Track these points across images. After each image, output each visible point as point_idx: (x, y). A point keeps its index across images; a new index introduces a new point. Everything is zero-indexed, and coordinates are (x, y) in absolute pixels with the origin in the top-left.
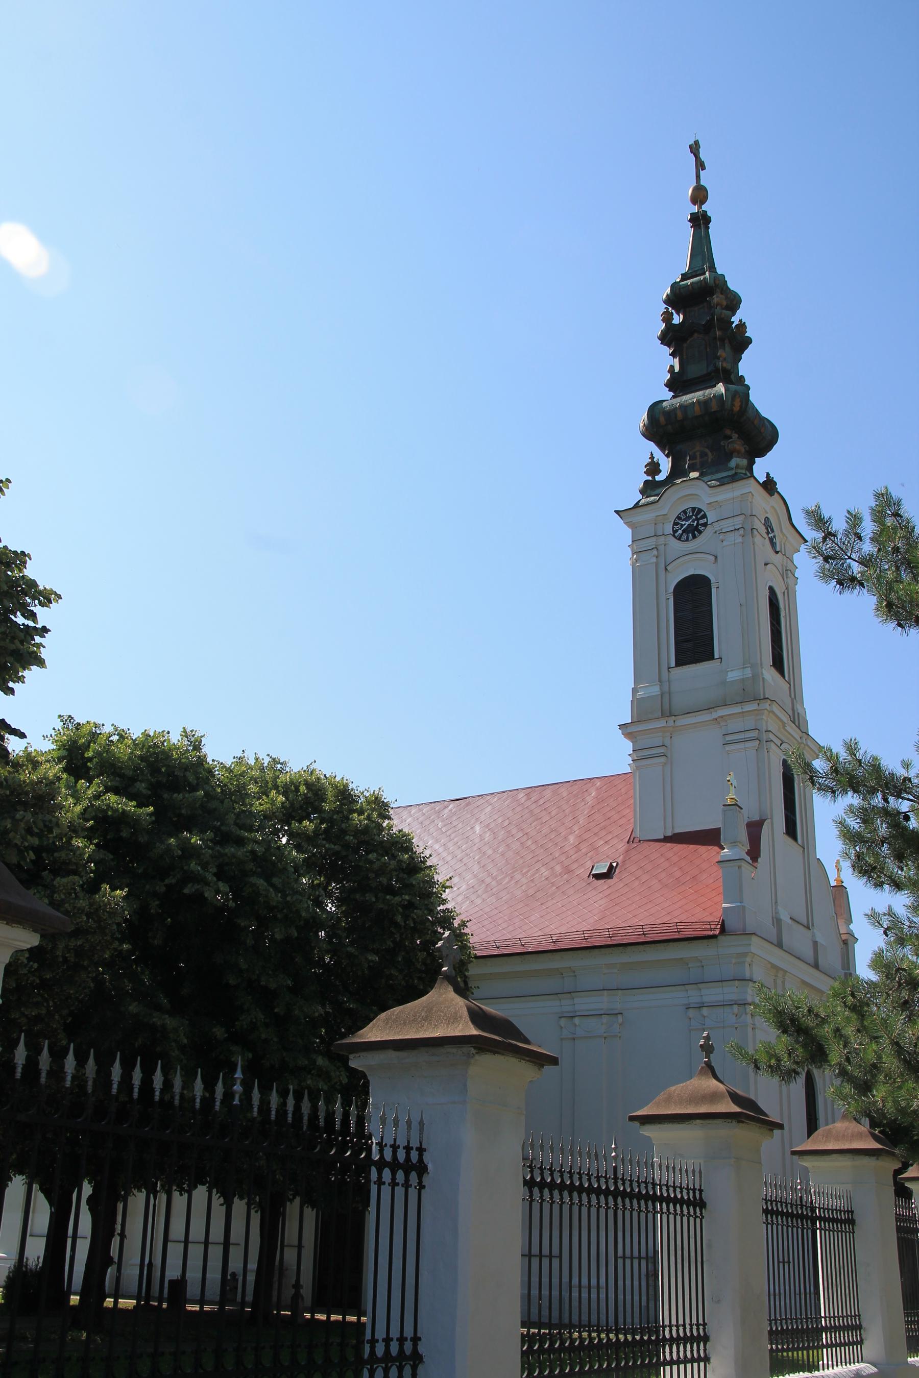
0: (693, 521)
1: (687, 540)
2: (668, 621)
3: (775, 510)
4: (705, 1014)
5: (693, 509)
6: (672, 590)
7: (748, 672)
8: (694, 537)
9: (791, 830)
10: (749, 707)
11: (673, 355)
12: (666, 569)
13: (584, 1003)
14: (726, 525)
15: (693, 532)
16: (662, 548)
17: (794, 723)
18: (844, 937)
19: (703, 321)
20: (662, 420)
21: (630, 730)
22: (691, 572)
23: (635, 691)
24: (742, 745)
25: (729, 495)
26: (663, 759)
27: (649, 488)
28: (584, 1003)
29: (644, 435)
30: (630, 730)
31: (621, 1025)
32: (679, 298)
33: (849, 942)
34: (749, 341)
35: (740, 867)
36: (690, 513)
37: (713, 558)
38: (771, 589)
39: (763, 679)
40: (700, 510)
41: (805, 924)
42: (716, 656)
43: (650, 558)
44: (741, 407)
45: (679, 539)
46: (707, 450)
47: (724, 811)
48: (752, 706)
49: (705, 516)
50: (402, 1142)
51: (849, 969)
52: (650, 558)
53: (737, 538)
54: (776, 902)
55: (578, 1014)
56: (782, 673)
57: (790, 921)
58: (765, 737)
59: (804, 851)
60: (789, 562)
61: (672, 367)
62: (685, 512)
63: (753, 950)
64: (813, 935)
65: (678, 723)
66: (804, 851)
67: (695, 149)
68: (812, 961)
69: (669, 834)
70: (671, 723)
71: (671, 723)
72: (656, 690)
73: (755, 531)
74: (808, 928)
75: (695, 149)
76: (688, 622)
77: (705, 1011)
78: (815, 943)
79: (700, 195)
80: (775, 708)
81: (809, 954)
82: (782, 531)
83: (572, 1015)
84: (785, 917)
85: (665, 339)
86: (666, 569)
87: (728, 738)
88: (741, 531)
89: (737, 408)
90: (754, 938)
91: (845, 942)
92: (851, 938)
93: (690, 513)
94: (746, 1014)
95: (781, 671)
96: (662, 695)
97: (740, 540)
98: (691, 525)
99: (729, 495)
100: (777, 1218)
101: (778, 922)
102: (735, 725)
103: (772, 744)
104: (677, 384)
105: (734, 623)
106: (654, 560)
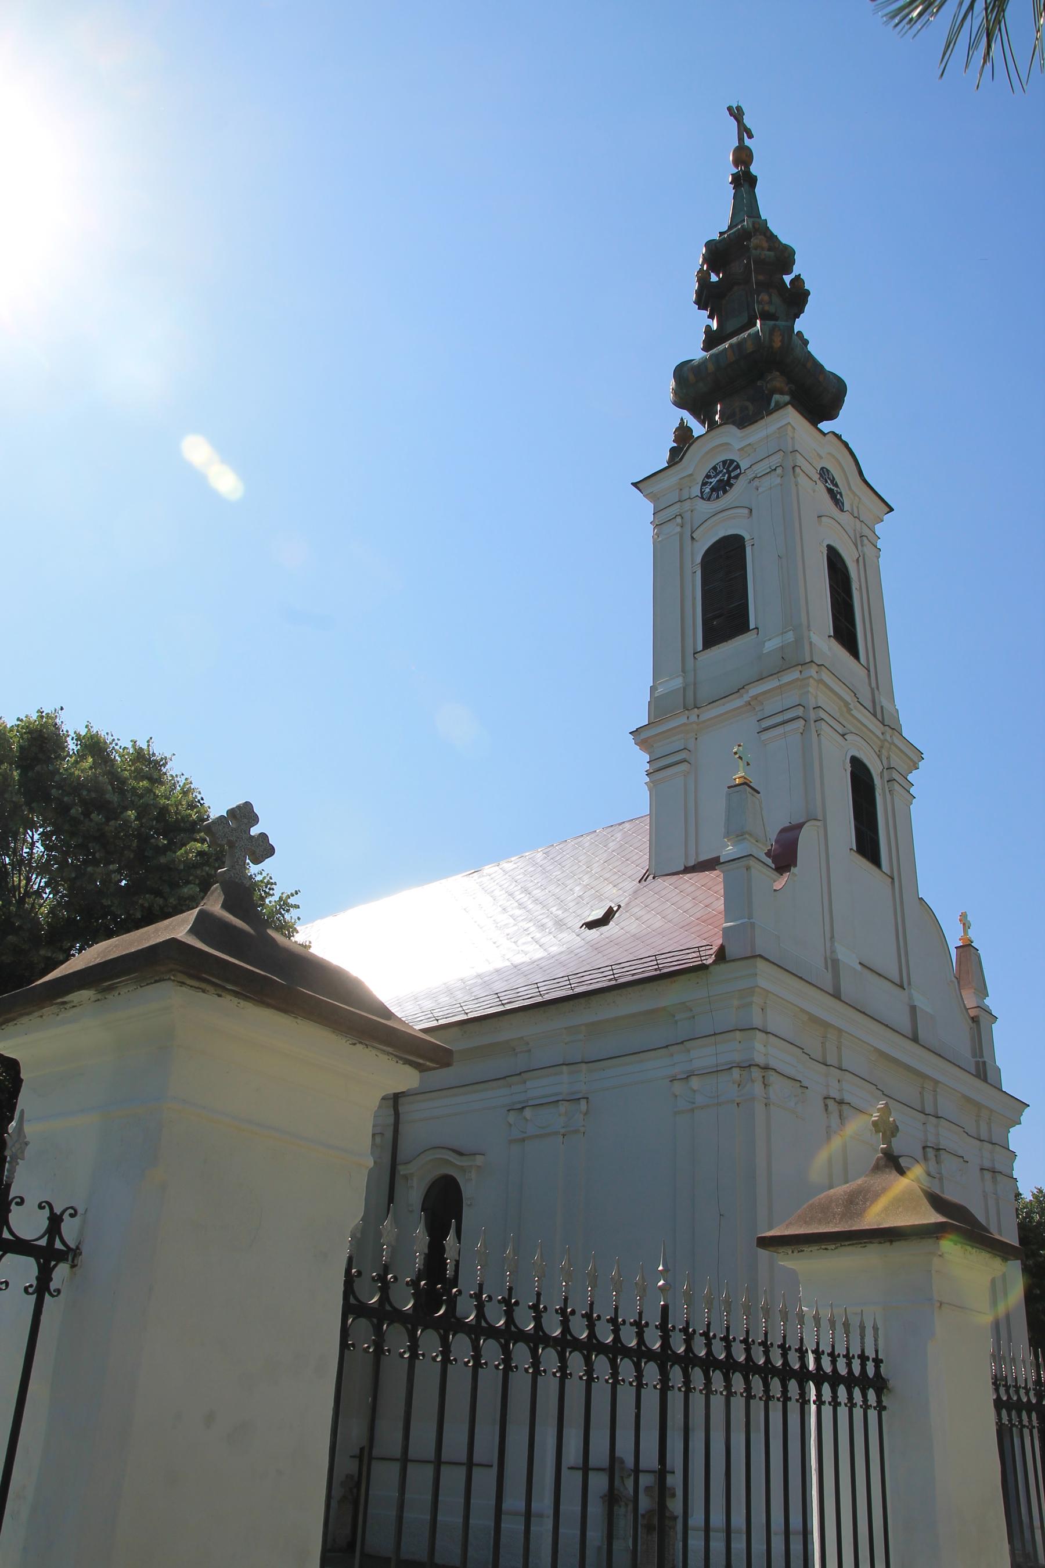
0: (724, 475)
1: (718, 497)
2: (694, 598)
3: (834, 457)
4: (695, 1088)
5: (724, 462)
6: (699, 559)
7: (790, 637)
8: (725, 492)
9: (868, 845)
10: (788, 677)
11: (711, 317)
12: (693, 538)
13: (539, 1087)
14: (761, 468)
15: (724, 486)
16: (687, 516)
17: (875, 715)
18: (972, 1013)
19: (748, 276)
20: (692, 378)
21: (644, 735)
22: (722, 533)
23: (653, 689)
24: (780, 730)
25: (763, 434)
26: (683, 767)
27: (676, 455)
28: (539, 1087)
29: (676, 404)
30: (644, 735)
31: (585, 1114)
32: (717, 254)
33: (982, 1020)
34: (807, 293)
35: (748, 868)
36: (720, 468)
37: (746, 511)
38: (831, 549)
39: (811, 643)
40: (732, 461)
41: (897, 980)
42: (752, 626)
43: (674, 529)
44: (782, 341)
45: (709, 500)
46: (748, 404)
47: (729, 795)
48: (793, 675)
49: (738, 467)
50: (855, 1351)
51: (982, 1056)
52: (674, 529)
53: (775, 480)
54: (832, 937)
55: (531, 1103)
56: (854, 653)
57: (859, 967)
58: (813, 716)
59: (893, 882)
60: (864, 527)
61: (708, 327)
62: (715, 468)
63: (762, 982)
64: (910, 998)
65: (702, 718)
66: (893, 882)
67: (737, 114)
68: (907, 1029)
69: (691, 863)
70: (693, 718)
71: (693, 718)
72: (678, 683)
73: (797, 469)
74: (902, 987)
75: (737, 114)
76: (719, 594)
77: (695, 1083)
78: (913, 1009)
79: (743, 156)
80: (826, 676)
81: (903, 1021)
82: (850, 488)
83: (519, 1106)
84: (848, 957)
85: (702, 301)
86: (693, 538)
87: (766, 724)
88: (779, 471)
89: (777, 344)
90: (760, 964)
91: (975, 1020)
92: (982, 1014)
93: (720, 468)
94: (753, 1081)
95: (851, 646)
96: (684, 689)
97: (778, 480)
98: (723, 479)
99: (763, 434)
100: (1020, 1416)
101: (834, 964)
102: (771, 706)
103: (824, 725)
104: (711, 340)
105: (785, 595)
106: (678, 529)
